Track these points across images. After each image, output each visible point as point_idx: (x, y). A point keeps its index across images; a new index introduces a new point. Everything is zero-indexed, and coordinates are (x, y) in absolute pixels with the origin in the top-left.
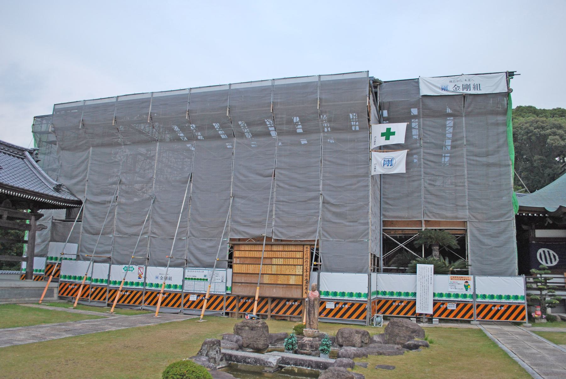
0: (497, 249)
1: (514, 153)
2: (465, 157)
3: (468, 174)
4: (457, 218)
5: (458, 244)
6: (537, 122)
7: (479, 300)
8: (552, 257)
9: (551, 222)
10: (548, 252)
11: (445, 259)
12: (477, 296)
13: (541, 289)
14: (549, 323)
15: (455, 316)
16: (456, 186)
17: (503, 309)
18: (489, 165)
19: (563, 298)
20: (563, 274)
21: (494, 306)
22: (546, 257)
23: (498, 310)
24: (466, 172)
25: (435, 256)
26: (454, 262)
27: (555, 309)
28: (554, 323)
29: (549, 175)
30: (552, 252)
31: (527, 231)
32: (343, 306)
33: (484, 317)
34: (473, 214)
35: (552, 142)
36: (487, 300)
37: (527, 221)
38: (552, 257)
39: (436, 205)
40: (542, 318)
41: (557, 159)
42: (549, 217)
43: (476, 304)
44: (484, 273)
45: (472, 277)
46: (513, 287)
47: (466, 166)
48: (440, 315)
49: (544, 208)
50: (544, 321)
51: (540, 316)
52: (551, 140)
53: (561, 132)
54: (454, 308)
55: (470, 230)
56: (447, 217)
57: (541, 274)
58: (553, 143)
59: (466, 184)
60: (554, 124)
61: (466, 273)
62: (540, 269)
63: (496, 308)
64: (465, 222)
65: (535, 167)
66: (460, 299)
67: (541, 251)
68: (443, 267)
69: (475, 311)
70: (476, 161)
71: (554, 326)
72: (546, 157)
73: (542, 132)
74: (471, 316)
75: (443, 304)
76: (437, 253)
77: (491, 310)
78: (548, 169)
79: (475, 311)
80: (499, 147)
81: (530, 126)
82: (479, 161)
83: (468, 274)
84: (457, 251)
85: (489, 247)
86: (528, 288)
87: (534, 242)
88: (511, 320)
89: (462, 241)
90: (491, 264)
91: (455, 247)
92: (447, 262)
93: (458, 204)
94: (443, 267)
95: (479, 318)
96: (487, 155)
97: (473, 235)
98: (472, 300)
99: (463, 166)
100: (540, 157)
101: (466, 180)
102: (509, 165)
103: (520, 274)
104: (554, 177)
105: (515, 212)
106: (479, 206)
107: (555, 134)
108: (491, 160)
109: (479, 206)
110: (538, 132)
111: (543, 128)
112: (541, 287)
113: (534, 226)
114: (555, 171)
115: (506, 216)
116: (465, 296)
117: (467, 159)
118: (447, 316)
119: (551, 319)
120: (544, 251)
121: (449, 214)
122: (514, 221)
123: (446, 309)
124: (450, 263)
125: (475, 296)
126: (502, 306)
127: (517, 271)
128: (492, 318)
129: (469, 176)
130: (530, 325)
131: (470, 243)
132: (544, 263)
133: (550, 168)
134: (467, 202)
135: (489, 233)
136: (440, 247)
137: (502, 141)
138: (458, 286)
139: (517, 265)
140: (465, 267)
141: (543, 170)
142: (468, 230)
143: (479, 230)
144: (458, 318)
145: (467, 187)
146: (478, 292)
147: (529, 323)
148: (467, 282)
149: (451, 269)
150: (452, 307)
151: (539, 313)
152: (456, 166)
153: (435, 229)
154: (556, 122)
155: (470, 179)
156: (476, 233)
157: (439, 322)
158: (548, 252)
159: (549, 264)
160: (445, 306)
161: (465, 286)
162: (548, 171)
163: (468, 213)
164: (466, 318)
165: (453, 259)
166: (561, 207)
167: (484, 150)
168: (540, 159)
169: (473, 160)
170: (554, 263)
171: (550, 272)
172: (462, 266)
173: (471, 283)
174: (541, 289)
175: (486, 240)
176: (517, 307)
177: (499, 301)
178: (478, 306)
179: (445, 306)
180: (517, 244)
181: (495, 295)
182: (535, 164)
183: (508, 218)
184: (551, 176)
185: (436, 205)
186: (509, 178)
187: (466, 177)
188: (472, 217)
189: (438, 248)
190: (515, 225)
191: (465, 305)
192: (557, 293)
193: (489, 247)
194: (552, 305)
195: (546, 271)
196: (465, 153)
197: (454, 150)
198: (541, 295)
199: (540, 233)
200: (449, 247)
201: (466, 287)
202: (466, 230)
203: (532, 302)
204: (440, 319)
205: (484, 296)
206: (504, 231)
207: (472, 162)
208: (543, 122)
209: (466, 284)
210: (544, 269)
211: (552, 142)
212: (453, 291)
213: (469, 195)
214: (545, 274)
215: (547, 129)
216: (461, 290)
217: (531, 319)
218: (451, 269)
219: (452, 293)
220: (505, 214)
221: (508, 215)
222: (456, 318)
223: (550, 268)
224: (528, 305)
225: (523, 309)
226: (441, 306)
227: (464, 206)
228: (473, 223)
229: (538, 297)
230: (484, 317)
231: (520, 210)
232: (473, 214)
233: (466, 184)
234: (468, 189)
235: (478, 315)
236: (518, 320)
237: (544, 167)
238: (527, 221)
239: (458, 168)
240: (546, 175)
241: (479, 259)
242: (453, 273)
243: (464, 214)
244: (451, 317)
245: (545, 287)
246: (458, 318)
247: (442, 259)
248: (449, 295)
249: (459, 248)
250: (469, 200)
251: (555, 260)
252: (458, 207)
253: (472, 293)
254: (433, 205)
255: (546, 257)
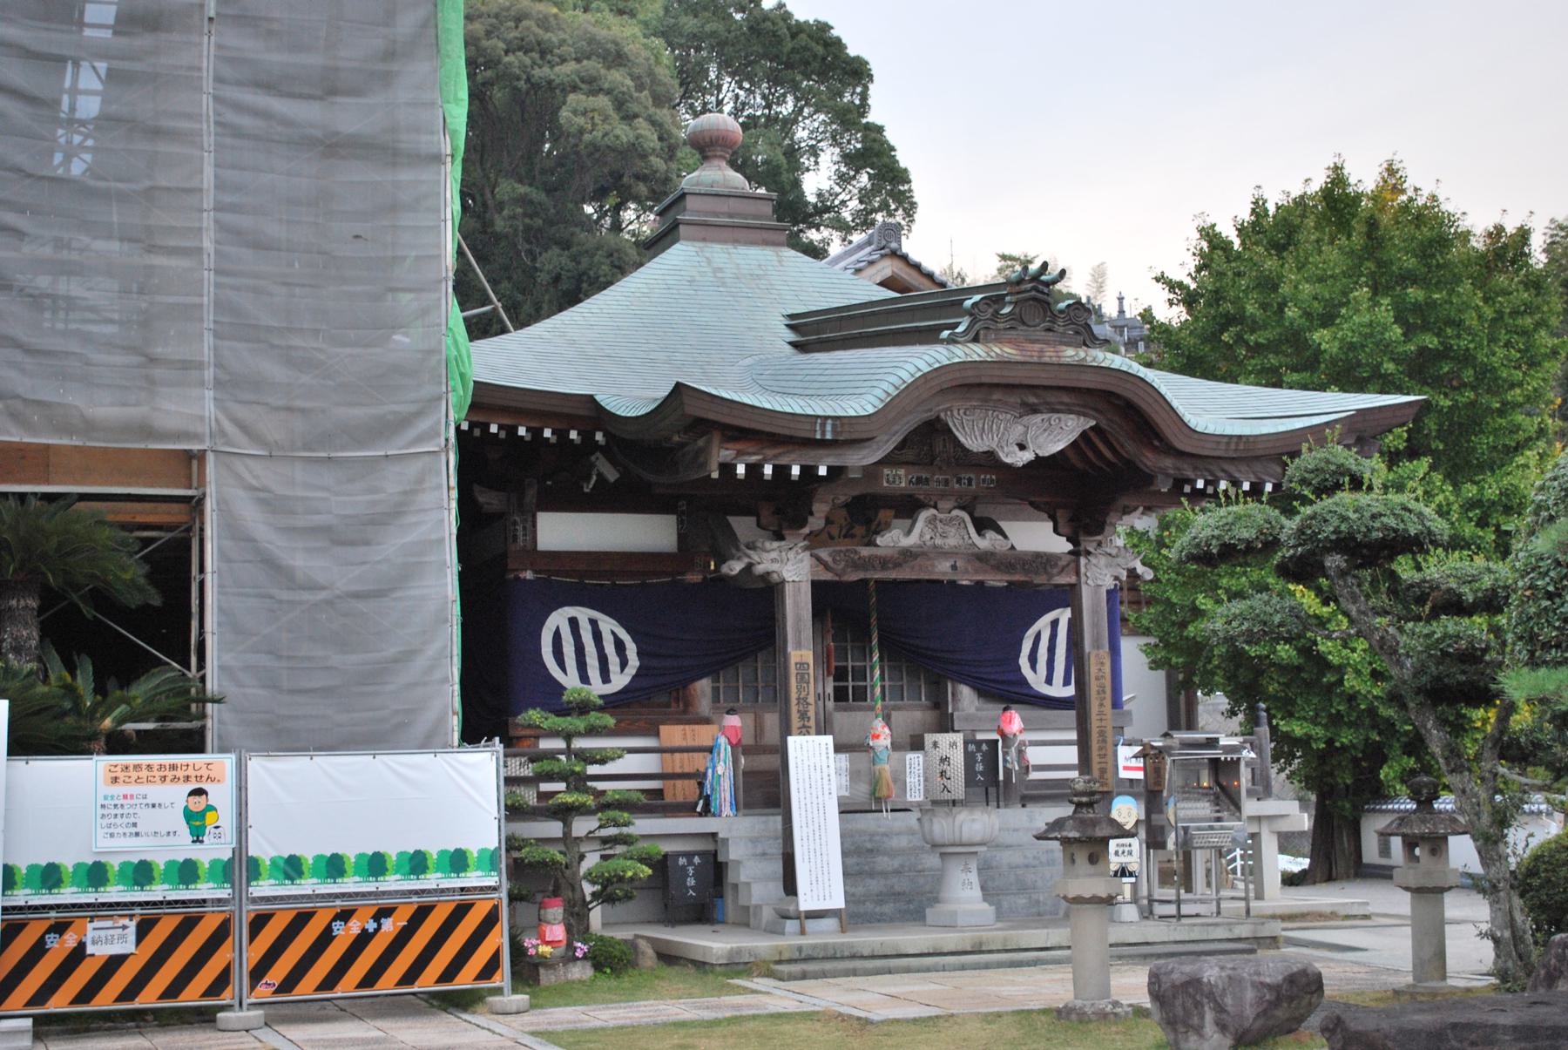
0: (361, 606)
1: (464, 94)
2: (208, 85)
3: (220, 186)
4: (147, 431)
5: (150, 577)
6: (518, 20)
7: (265, 887)
8: (610, 649)
9: (612, 475)
10: (594, 623)
11: (72, 669)
12: (254, 869)
13: (565, 813)
14: (607, 982)
15: (130, 993)
16: (152, 249)
17: (390, 926)
18: (334, 147)
19: (666, 847)
20: (657, 734)
21: (345, 915)
22: (584, 650)
23: (364, 939)
24: (209, 173)
25: (17, 650)
26: (126, 682)
27: (620, 909)
28: (626, 982)
29: (557, 279)
30: (608, 625)
31: (500, 516)
32: (371, 926)
33: (288, 985)
34: (242, 412)
35: (581, 120)
36: (307, 886)
37: (517, 458)
38: (610, 649)
39: (29, 351)
40: (570, 958)
41: (589, 209)
42: (605, 450)
43: (249, 910)
44: (287, 739)
45: (228, 761)
46: (447, 802)
47: (209, 141)
48: (41, 997)
49: (591, 398)
50: (581, 972)
51: (562, 949)
52: (575, 112)
53: (618, 77)
54: (128, 946)
55: (222, 502)
56: (90, 427)
57: (568, 737)
58: (581, 131)
59: (208, 244)
60: (592, 40)
61: (193, 742)
62: (563, 711)
63: (354, 927)
64: (190, 462)
65: (498, 237)
66: (157, 892)
67: (558, 619)
68: (65, 714)
69: (243, 953)
70: (266, 115)
71: (630, 995)
72: (550, 190)
73: (537, 72)
74: (221, 983)
75: (60, 928)
76: (30, 634)
77: (326, 938)
78: (556, 250)
79: (243, 953)
80: (390, 54)
81: (488, 34)
82: (287, 122)
83: (200, 749)
84: (140, 619)
85: (322, 595)
86: (514, 811)
87: (529, 575)
88: (427, 982)
89: (173, 563)
90: (327, 691)
91: (134, 600)
92: (84, 683)
93: (159, 350)
94: (65, 714)
95: (264, 992)
96: (329, 87)
97: (232, 529)
98: (224, 893)
99: (192, 138)
100: (522, 189)
101: (208, 220)
102: (437, 159)
103: (472, 735)
104: (579, 289)
105: (453, 412)
106: (273, 370)
107: (592, 85)
108: (348, 117)
109: (273, 370)
110: (523, 67)
111: (544, 51)
112: (569, 799)
113: (531, 495)
114: (585, 261)
115: (412, 433)
116: (187, 872)
117: (217, 99)
118: (86, 995)
119: (611, 962)
120: (573, 623)
121: (104, 408)
122: (453, 459)
123: (78, 954)
124: (100, 689)
125: (241, 867)
126: (383, 913)
127: (455, 723)
128: (329, 983)
129: (228, 199)
130: (522, 999)
131: (218, 572)
132: (569, 680)
133: (566, 245)
134: (208, 339)
135: (318, 520)
136: (48, 597)
137: (406, 24)
138: (147, 821)
139: (457, 687)
140: (184, 713)
141: (530, 252)
142: (209, 505)
143: (271, 503)
144: (148, 999)
145: (209, 261)
146: (262, 847)
147: (515, 991)
148: (199, 792)
149: (108, 723)
150: (109, 940)
151: (557, 932)
152: (156, 133)
153: (22, 497)
154: (602, 33)
155: (228, 218)
156: (252, 517)
157: (38, 1036)
158: (594, 623)
159: (597, 688)
160: (70, 940)
161: (189, 815)
162: (552, 260)
163: (210, 409)
164: (191, 997)
165: (119, 668)
166: (678, 386)
167: (314, 60)
168: (523, 201)
169: (255, 112)
170: (620, 681)
171: (610, 721)
172: (175, 702)
173: (221, 796)
174: (565, 813)
175: (301, 561)
176: (461, 911)
177: (369, 887)
178: (259, 923)
179: (70, 940)
180: (462, 576)
181: (308, 855)
182: (500, 224)
183: (419, 439)
184: (564, 286)
185: (29, 351)
186: (437, 229)
187: (208, 202)
188: (229, 427)
189: (33, 603)
190: (453, 482)
191: (189, 924)
192: (643, 825)
193: (322, 595)
194: (611, 890)
195: (594, 718)
196: (208, 65)
197: (144, 41)
198: (567, 839)
199: (560, 531)
200: (102, 598)
201: (196, 822)
202: (195, 505)
203: (532, 876)
204: (39, 1020)
205: (292, 867)
206: (393, 514)
207: (246, 122)
208: (544, 23)
209: (198, 804)
210: (583, 708)
211: (581, 120)
212: (119, 849)
213: (219, 305)
214: (592, 732)
215: (563, 60)
216: (165, 842)
217: (527, 971)
218: (108, 723)
219: (114, 863)
220: (404, 422)
221: (423, 425)
222: (136, 1004)
223: (611, 703)
224: (513, 898)
225: (491, 920)
226: (51, 939)
227: (189, 365)
228: (239, 465)
229: (554, 853)
230: (288, 985)
231: (474, 407)
232: (242, 412)
233: (208, 244)
234: (218, 272)
235: (258, 974)
236: (465, 981)
237: (537, 238)
238: (517, 458)
239: (163, 147)
240: (543, 278)
241: (265, 660)
242: (117, 744)
243: (189, 411)
244: (105, 1001)
245: (589, 800)
246: (148, 999)
247: (57, 671)
248: (96, 874)
249: (157, 601)
250: (217, 335)
251: (624, 664)
252: (158, 372)
253: (226, 855)
254: (18, 356)
255: (584, 650)
